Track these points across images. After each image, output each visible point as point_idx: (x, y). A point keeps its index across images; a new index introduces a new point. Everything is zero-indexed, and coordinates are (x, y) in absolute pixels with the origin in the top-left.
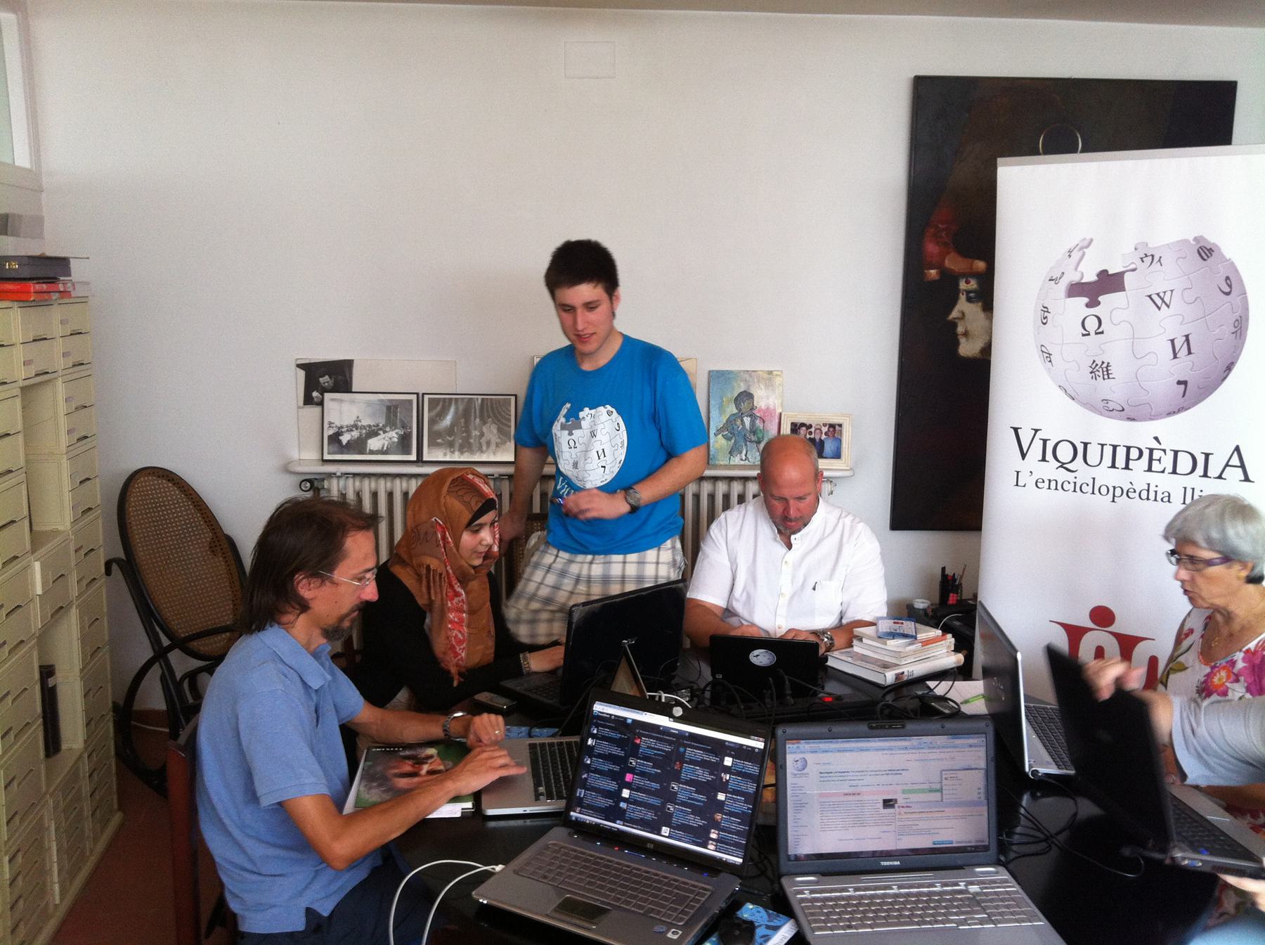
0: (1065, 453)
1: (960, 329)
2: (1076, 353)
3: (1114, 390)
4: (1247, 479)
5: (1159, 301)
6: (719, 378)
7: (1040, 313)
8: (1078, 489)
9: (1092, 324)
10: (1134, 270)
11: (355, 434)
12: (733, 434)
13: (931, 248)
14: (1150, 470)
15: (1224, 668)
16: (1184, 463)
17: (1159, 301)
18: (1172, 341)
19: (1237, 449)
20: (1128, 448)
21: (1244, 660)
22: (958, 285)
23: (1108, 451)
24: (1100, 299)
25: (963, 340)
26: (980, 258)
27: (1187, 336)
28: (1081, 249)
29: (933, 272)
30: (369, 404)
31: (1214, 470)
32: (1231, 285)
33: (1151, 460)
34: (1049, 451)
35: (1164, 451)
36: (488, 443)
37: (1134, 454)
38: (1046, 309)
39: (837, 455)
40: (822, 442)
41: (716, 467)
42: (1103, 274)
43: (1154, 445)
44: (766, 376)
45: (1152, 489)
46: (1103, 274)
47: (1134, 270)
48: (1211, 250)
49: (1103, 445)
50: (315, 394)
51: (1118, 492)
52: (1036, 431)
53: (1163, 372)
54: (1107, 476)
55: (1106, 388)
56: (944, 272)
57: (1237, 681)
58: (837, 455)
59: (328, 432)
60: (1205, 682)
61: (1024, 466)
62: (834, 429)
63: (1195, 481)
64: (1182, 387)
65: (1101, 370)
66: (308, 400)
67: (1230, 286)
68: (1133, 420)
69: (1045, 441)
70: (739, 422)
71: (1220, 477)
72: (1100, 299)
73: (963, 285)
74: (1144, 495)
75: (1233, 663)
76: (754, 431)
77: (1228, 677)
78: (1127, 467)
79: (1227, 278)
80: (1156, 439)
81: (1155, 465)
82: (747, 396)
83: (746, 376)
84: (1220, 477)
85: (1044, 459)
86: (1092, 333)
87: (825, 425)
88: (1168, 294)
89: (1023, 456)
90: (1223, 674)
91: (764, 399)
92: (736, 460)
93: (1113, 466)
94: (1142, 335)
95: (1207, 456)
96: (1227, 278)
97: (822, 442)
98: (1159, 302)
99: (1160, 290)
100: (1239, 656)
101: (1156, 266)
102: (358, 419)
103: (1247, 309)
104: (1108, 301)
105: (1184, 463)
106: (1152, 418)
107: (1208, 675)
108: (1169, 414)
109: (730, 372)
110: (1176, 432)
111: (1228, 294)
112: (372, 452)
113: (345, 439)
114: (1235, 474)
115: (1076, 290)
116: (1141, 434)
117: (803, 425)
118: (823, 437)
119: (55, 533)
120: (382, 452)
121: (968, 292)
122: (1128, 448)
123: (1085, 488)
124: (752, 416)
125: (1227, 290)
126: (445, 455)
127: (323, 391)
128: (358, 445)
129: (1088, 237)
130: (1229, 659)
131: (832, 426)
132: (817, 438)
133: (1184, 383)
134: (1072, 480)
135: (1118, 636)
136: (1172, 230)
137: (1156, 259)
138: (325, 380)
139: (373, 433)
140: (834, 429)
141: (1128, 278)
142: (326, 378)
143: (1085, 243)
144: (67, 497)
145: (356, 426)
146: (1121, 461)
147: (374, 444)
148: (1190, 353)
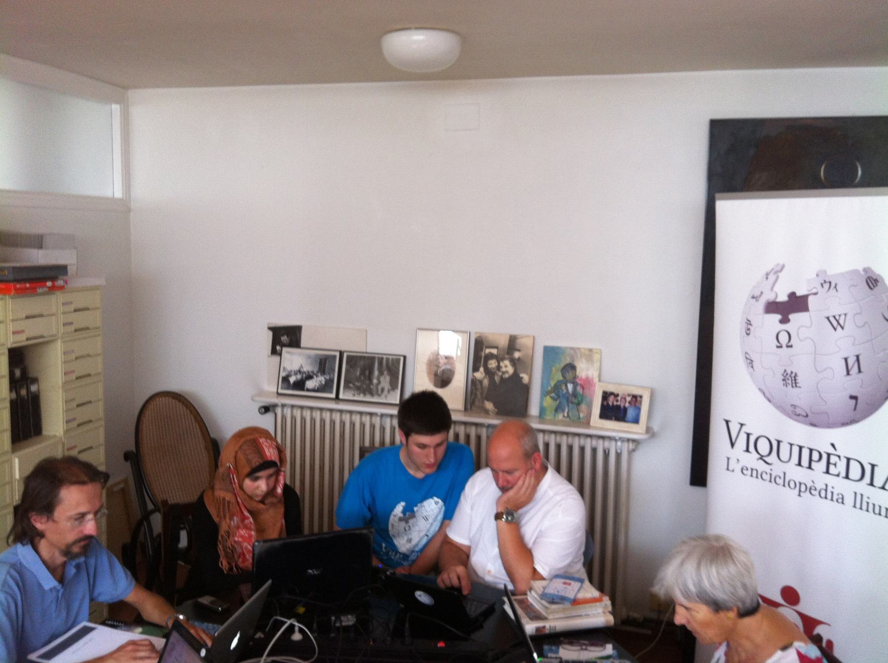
0: (763, 446)
3: (800, 396)
5: (835, 323)
6: (551, 353)
9: (784, 338)
10: (816, 294)
11: (299, 377)
12: (559, 396)
14: (827, 472)
16: (855, 472)
17: (835, 323)
18: (846, 360)
23: (796, 450)
27: (858, 357)
28: (776, 272)
30: (309, 357)
33: (828, 463)
34: (751, 445)
36: (383, 390)
37: (815, 456)
38: (749, 322)
39: (636, 421)
40: (625, 409)
42: (792, 295)
43: (831, 450)
44: (587, 352)
45: (830, 489)
46: (792, 295)
47: (816, 294)
48: (876, 281)
49: (791, 445)
50: (278, 348)
52: (742, 425)
53: (837, 387)
55: (795, 396)
58: (636, 421)
59: (283, 374)
62: (636, 399)
63: (863, 487)
64: (854, 401)
65: (790, 379)
66: (274, 352)
69: (748, 435)
70: (564, 387)
72: (792, 317)
76: (575, 394)
78: (810, 467)
80: (833, 445)
81: (832, 469)
82: (571, 367)
85: (747, 450)
86: (784, 346)
87: (629, 395)
89: (732, 445)
91: (584, 370)
92: (560, 417)
93: (799, 464)
94: (822, 350)
97: (625, 409)
98: (835, 323)
99: (836, 313)
101: (832, 291)
102: (302, 366)
104: (796, 318)
105: (855, 472)
108: (844, 424)
109: (558, 348)
112: (308, 390)
113: (292, 379)
115: (772, 307)
116: (821, 439)
117: (612, 394)
118: (627, 405)
119: (55, 436)
120: (314, 390)
122: (811, 450)
123: (778, 480)
124: (575, 385)
126: (354, 395)
127: (283, 345)
128: (300, 385)
129: (781, 263)
131: (635, 397)
132: (622, 405)
133: (854, 398)
134: (769, 471)
135: (803, 617)
136: (845, 261)
137: (833, 285)
138: (284, 339)
139: (309, 377)
140: (636, 399)
141: (811, 300)
142: (286, 337)
143: (779, 268)
144: (61, 416)
145: (300, 371)
147: (310, 384)
148: (860, 371)
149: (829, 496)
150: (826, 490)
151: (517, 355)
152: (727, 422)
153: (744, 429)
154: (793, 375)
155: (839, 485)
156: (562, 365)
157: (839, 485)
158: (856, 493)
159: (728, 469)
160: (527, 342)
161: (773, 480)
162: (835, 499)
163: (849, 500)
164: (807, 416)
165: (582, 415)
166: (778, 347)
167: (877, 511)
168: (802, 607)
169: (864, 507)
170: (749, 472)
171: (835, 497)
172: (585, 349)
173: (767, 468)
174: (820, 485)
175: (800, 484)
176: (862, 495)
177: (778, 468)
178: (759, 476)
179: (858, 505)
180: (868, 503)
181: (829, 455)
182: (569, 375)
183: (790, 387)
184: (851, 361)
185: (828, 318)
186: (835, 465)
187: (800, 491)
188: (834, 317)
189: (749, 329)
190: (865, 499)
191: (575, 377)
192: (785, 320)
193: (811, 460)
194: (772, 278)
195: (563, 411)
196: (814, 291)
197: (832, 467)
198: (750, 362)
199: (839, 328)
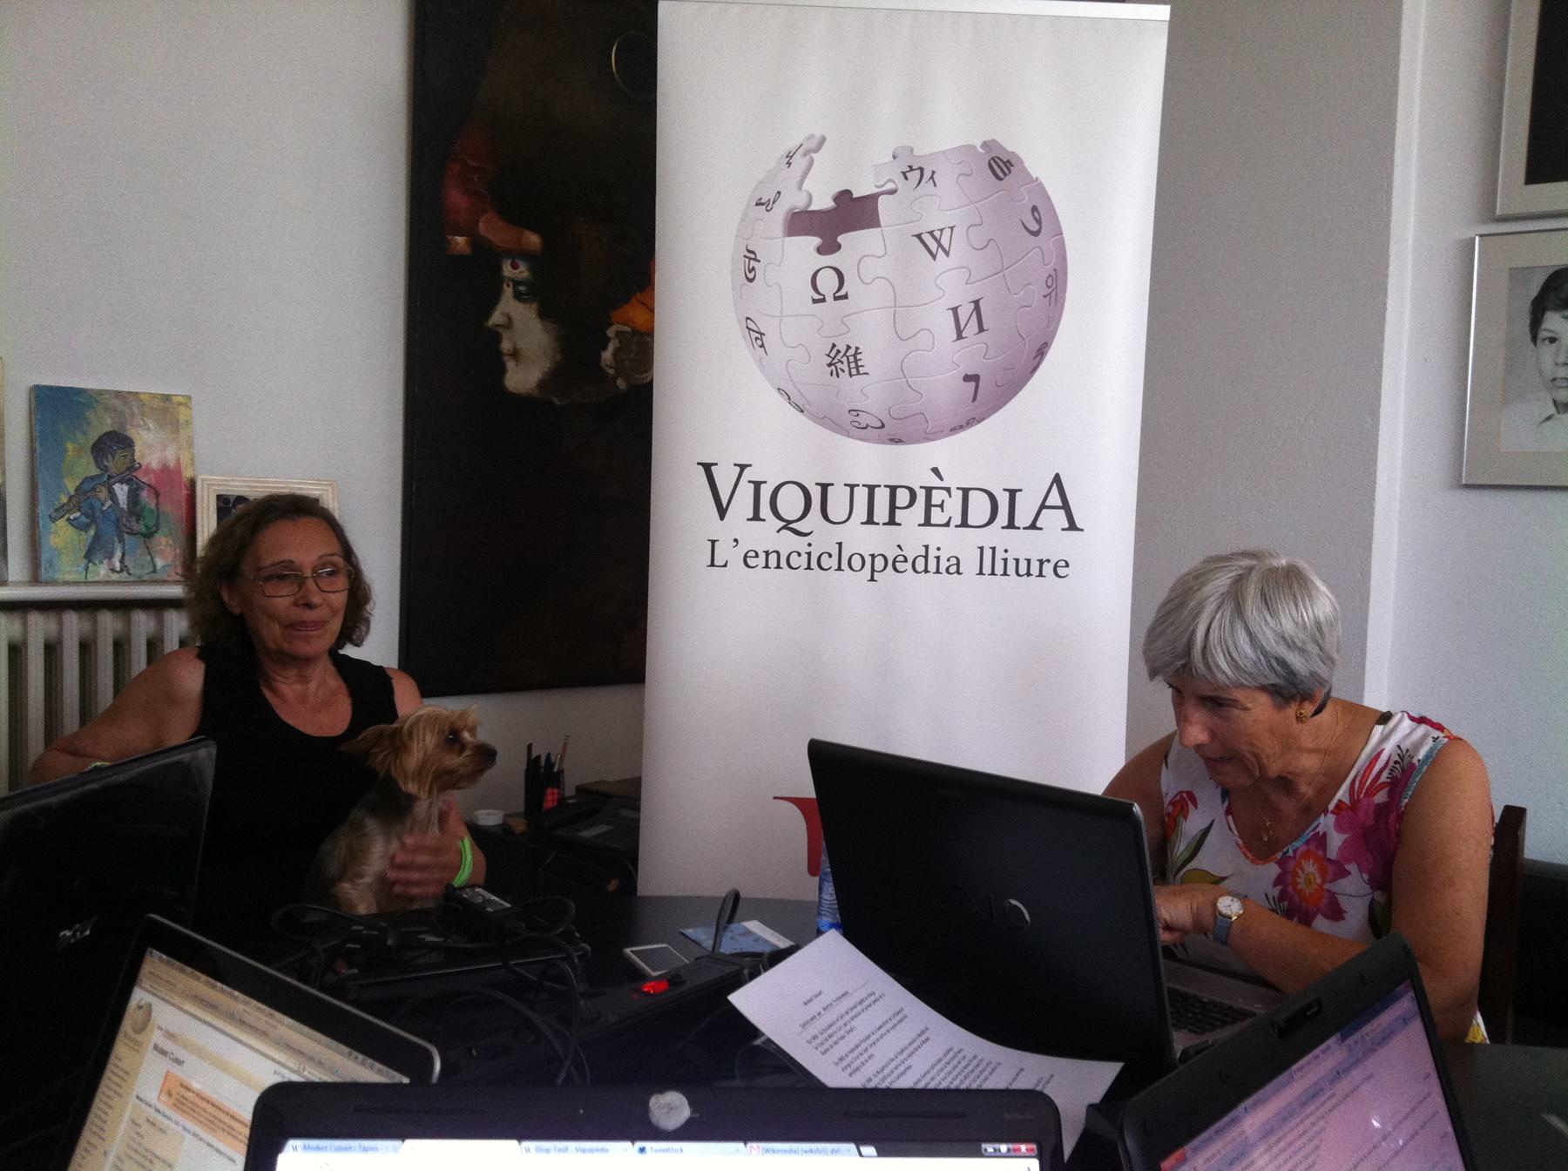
0: (791, 503)
1: (506, 346)
2: (799, 329)
3: (868, 392)
4: (1072, 526)
5: (931, 243)
7: (741, 264)
8: (814, 564)
9: (828, 282)
10: (892, 192)
13: (457, 199)
15: (1306, 855)
16: (979, 508)
17: (931, 243)
18: (955, 310)
19: (1057, 480)
20: (893, 490)
21: (1339, 827)
22: (500, 269)
23: (861, 495)
24: (840, 239)
25: (510, 364)
26: (535, 230)
27: (976, 303)
29: (460, 239)
31: (1023, 517)
32: (1039, 220)
33: (929, 506)
34: (765, 502)
35: (948, 490)
37: (903, 497)
38: (751, 255)
41: (52, 583)
42: (844, 197)
45: (933, 553)
46: (844, 197)
47: (892, 192)
48: (1008, 164)
49: (852, 487)
51: (879, 563)
52: (743, 467)
53: (943, 358)
54: (862, 539)
56: (477, 242)
57: (1344, 873)
60: (1283, 896)
61: (722, 531)
63: (995, 535)
65: (845, 360)
67: (1039, 222)
68: (899, 441)
69: (757, 485)
70: (103, 494)
71: (1033, 526)
72: (840, 239)
73: (507, 270)
74: (920, 565)
75: (1321, 840)
77: (1323, 872)
78: (892, 521)
79: (1035, 209)
80: (936, 471)
81: (937, 515)
82: (115, 443)
83: (118, 403)
84: (1033, 526)
85: (756, 517)
86: (829, 298)
88: (947, 232)
89: (722, 512)
90: (1310, 868)
92: (102, 571)
93: (870, 521)
95: (1013, 493)
96: (1035, 209)
99: (935, 226)
100: (1326, 822)
101: (927, 185)
103: (1065, 258)
105: (979, 508)
106: (928, 437)
107: (1279, 881)
110: (962, 458)
111: (1036, 234)
114: (1055, 519)
115: (801, 222)
116: (914, 464)
121: (516, 283)
122: (893, 490)
123: (825, 562)
125: (1035, 227)
129: (818, 134)
130: (1308, 834)
134: (804, 549)
137: (927, 175)
143: (813, 144)
146: (881, 513)
148: (981, 329)
149: (932, 566)
150: (926, 557)
152: (707, 468)
154: (851, 352)
155: (948, 542)
156: (94, 435)
157: (948, 542)
158: (982, 549)
159: (712, 565)
161: (815, 563)
162: (943, 569)
163: (970, 564)
164: (883, 426)
165: (159, 563)
166: (815, 301)
167: (1023, 570)
169: (999, 568)
170: (761, 560)
171: (944, 565)
172: (153, 396)
173: (800, 544)
175: (873, 556)
176: (994, 549)
177: (823, 537)
178: (781, 561)
179: (987, 569)
180: (1005, 560)
181: (929, 490)
182: (115, 463)
183: (844, 376)
184: (963, 315)
185: (919, 236)
186: (941, 506)
187: (873, 570)
188: (931, 233)
190: (1000, 555)
191: (133, 467)
192: (828, 247)
193: (893, 508)
194: (799, 162)
195: (110, 556)
196: (890, 186)
197: (935, 511)
198: (758, 338)
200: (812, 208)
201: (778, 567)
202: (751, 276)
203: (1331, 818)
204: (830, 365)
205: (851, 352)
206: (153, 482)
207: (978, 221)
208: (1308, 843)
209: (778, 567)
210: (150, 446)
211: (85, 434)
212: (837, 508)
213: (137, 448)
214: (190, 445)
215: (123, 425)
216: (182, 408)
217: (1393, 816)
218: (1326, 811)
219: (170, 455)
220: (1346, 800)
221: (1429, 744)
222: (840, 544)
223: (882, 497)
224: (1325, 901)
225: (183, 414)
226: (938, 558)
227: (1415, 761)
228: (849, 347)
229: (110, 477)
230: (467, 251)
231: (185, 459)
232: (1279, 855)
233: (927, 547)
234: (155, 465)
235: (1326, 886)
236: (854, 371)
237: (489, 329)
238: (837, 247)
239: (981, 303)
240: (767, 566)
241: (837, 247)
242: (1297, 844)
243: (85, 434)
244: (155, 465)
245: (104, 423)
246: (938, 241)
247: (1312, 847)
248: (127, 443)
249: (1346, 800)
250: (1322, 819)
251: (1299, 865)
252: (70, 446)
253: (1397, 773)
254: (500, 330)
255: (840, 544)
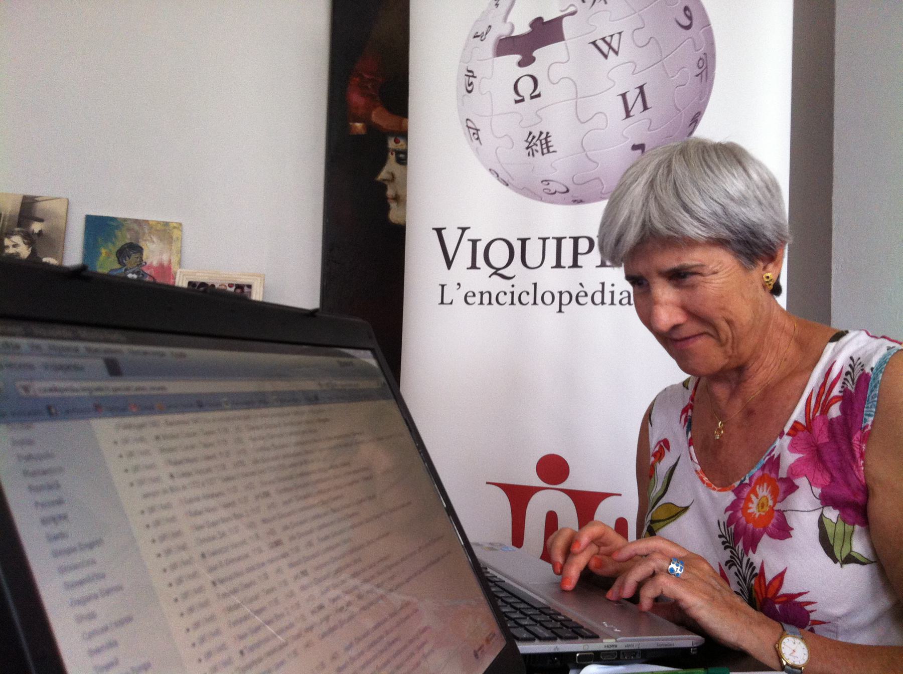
1: (390, 193)
2: (505, 122)
3: (556, 166)
7: (463, 80)
9: (526, 87)
13: (356, 99)
15: (761, 480)
17: (605, 47)
18: (624, 96)
20: (576, 240)
21: (793, 448)
22: (386, 143)
23: (551, 245)
24: (535, 54)
27: (641, 88)
37: (583, 245)
38: (471, 74)
42: (538, 23)
46: (538, 23)
49: (544, 240)
52: (464, 230)
54: (552, 280)
61: (450, 277)
65: (538, 143)
68: (581, 202)
69: (474, 242)
77: (774, 493)
78: (575, 265)
79: (686, 9)
80: (581, 284)
82: (134, 248)
83: (136, 227)
85: (474, 266)
86: (527, 98)
88: (616, 37)
89: (449, 263)
93: (558, 265)
96: (686, 9)
98: (605, 48)
99: (606, 34)
104: (546, 55)
107: (733, 507)
111: (688, 28)
115: (506, 46)
122: (576, 240)
123: (524, 298)
133: (640, 147)
134: (509, 289)
141: (566, 23)
146: (567, 259)
148: (645, 108)
149: (608, 299)
150: (603, 292)
151: (36, 227)
152: (439, 231)
153: (468, 235)
154: (543, 136)
156: (119, 244)
159: (442, 303)
160: (58, 207)
161: (516, 299)
162: (616, 301)
164: (568, 191)
166: (517, 102)
168: (573, 482)
171: (617, 298)
172: (158, 222)
173: (505, 285)
174: (592, 287)
178: (492, 299)
185: (594, 43)
187: (561, 304)
188: (603, 39)
189: (471, 84)
192: (526, 61)
193: (576, 254)
196: (572, 9)
199: (611, 53)
200: (514, 34)
201: (490, 303)
202: (470, 88)
203: (787, 440)
204: (527, 148)
205: (543, 136)
206: (153, 274)
207: (640, 25)
208: (763, 468)
209: (490, 303)
210: (153, 252)
211: (113, 243)
212: (533, 257)
213: (145, 253)
214: (180, 252)
215: (137, 239)
216: (175, 231)
217: (857, 436)
218: (781, 434)
219: (165, 258)
220: (803, 421)
221: (883, 351)
222: (535, 284)
223: (568, 246)
224: (774, 521)
225: (176, 234)
226: (612, 293)
227: (868, 370)
228: (541, 133)
229: (126, 270)
230: (363, 132)
231: (175, 260)
232: (737, 484)
233: (603, 284)
234: (155, 263)
235: (778, 507)
236: (545, 151)
237: (378, 182)
238: (533, 60)
239: (645, 88)
240: (481, 303)
241: (533, 60)
242: (754, 471)
243: (113, 243)
244: (155, 263)
245: (125, 238)
246: (609, 45)
247: (766, 471)
248: (139, 250)
249: (803, 421)
250: (778, 442)
251: (754, 491)
252: (103, 251)
253: (851, 387)
254: (386, 183)
255: (535, 284)
